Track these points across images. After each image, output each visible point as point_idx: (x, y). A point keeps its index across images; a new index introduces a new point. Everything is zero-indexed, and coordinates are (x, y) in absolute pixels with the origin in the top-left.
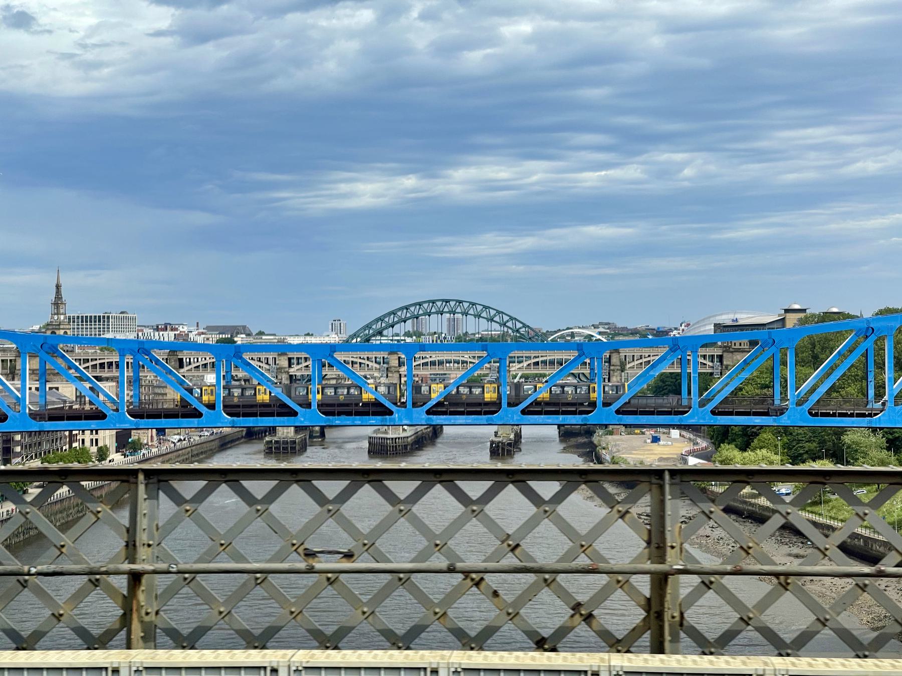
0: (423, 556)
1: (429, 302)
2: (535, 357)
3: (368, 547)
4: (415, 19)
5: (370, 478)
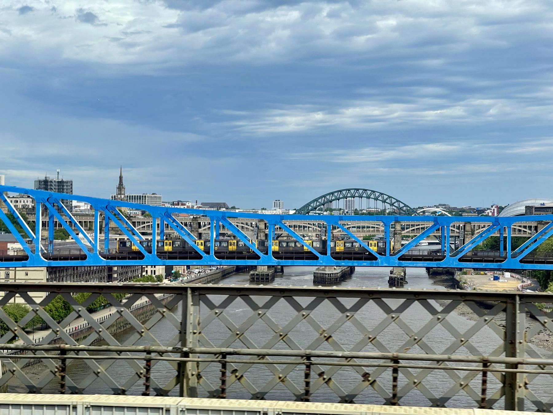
0: (452, 349)
1: (346, 190)
2: (417, 225)
3: (283, 337)
4: (325, 17)
5: (241, 294)
